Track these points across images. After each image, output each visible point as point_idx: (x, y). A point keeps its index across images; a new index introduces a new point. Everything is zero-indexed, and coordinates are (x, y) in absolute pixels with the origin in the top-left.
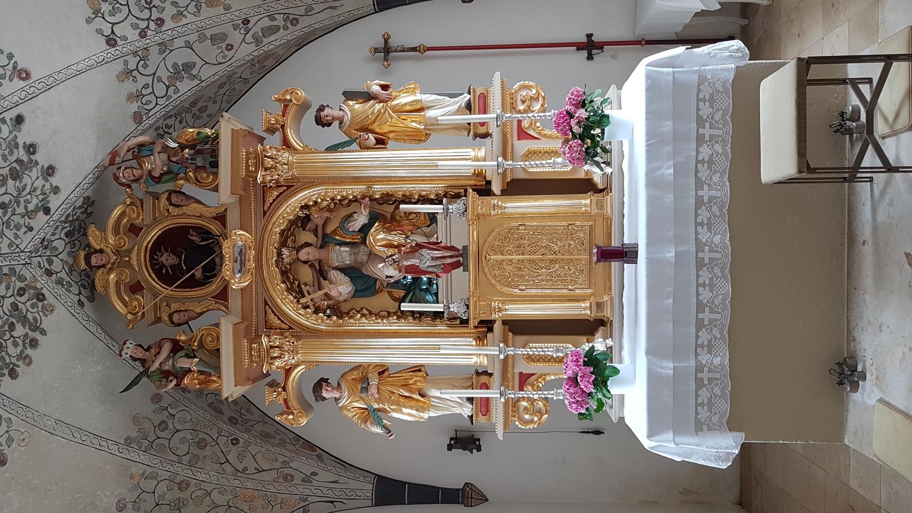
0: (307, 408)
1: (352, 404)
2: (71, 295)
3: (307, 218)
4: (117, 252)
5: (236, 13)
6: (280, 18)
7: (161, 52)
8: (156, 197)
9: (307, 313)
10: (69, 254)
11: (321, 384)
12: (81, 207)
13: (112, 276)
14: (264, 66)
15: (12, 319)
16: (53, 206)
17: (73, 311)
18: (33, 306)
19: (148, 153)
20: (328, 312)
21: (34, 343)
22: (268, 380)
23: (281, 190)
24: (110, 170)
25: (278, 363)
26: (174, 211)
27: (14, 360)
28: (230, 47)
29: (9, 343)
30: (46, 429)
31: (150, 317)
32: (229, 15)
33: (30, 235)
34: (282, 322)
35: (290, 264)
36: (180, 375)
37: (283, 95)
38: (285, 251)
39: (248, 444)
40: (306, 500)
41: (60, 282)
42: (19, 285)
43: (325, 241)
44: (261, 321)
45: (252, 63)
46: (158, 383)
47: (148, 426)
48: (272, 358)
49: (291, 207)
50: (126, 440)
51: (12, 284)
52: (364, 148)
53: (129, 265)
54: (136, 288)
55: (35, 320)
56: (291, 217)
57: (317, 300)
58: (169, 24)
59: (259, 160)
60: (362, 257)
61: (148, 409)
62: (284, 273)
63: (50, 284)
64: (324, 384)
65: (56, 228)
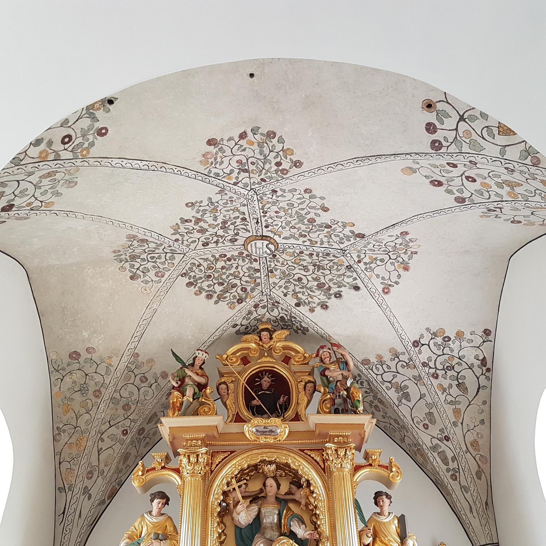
0: (146, 487)
1: (147, 524)
2: (241, 320)
3: (300, 486)
4: (270, 349)
5: (452, 431)
6: (455, 465)
7: (415, 377)
8: (311, 373)
9: (223, 485)
10: (269, 319)
11: (165, 498)
12: (301, 326)
13: (254, 345)
14: (416, 453)
15: (226, 284)
16: (301, 308)
17: (230, 320)
18: (234, 297)
19: (342, 368)
20: (224, 504)
21: (209, 297)
22: (171, 455)
23: (321, 464)
24: (326, 342)
25: (185, 460)
26: (301, 386)
27: (199, 285)
28: (426, 427)
29: (211, 282)
30: (151, 303)
31: (224, 370)
32: (450, 425)
33: (282, 295)
34: (217, 465)
35: (263, 473)
36: (181, 389)
37: (395, 465)
38: (273, 467)
39: (122, 442)
40: (70, 490)
41: (250, 313)
42: (249, 289)
43: (282, 502)
44: (219, 449)
45: (417, 445)
46: (176, 375)
47: (145, 369)
48: (189, 456)
49: (308, 472)
50: (137, 354)
51: (249, 284)
52: (360, 534)
53: (262, 356)
54: (245, 360)
55: (225, 298)
56: (300, 472)
57: (234, 494)
58: (435, 382)
59: (342, 445)
60: (269, 534)
61: (158, 369)
62: (255, 467)
63: (248, 307)
64: (164, 501)
65: (286, 311)
